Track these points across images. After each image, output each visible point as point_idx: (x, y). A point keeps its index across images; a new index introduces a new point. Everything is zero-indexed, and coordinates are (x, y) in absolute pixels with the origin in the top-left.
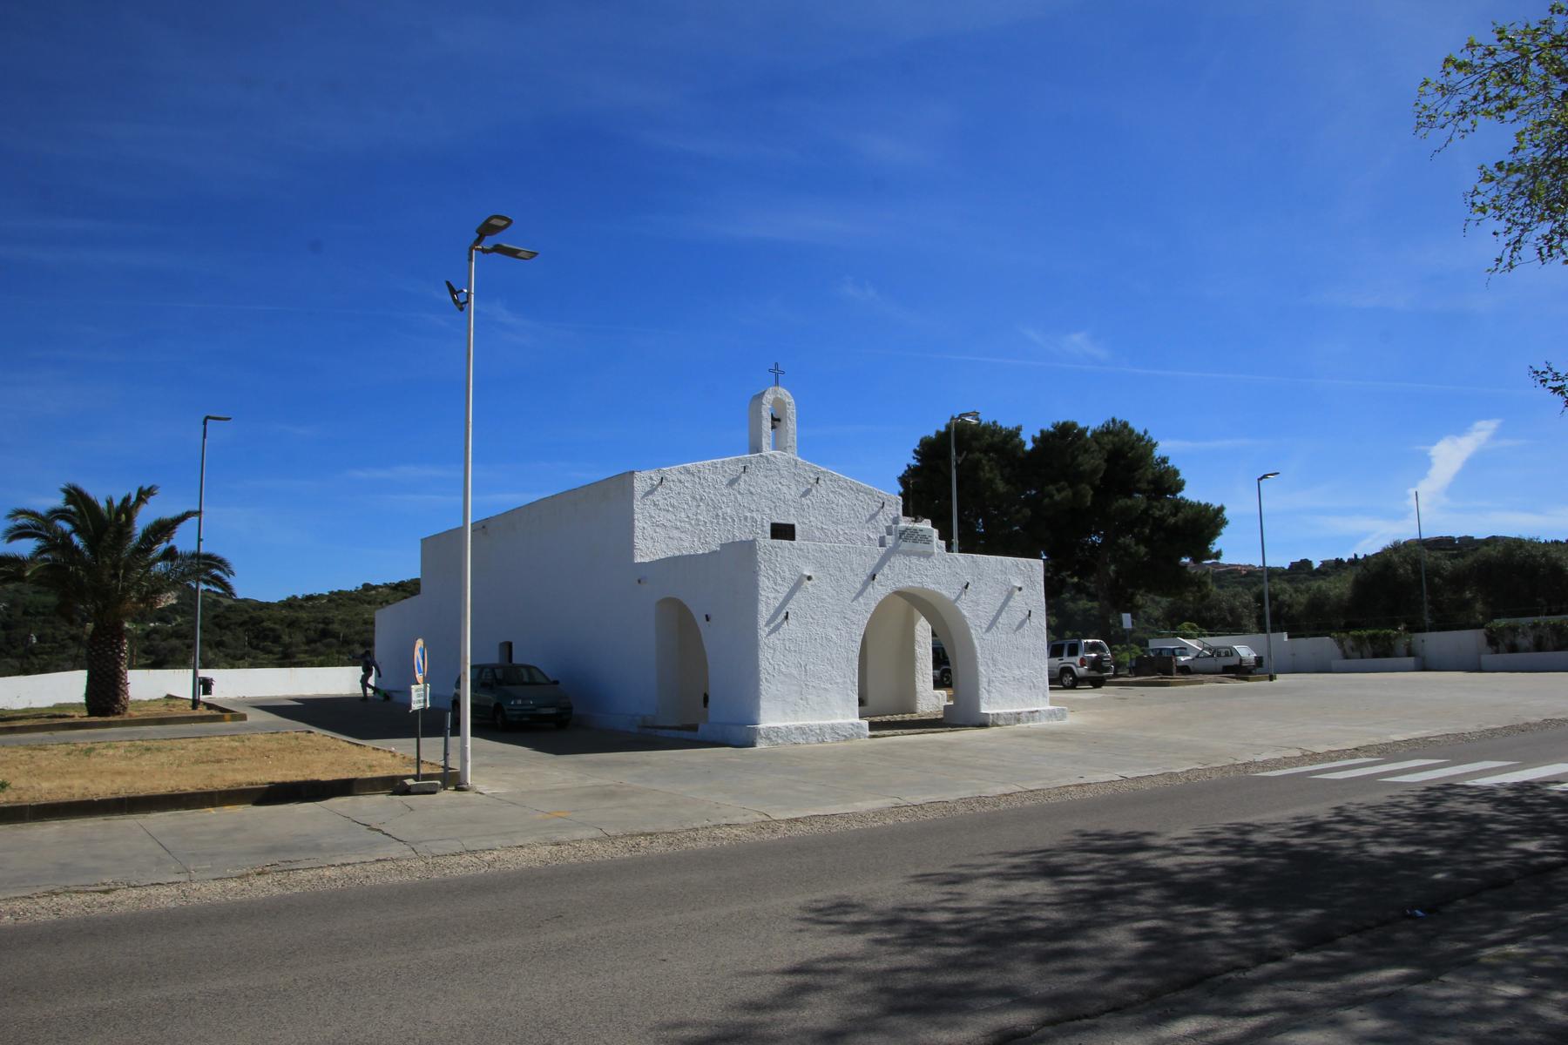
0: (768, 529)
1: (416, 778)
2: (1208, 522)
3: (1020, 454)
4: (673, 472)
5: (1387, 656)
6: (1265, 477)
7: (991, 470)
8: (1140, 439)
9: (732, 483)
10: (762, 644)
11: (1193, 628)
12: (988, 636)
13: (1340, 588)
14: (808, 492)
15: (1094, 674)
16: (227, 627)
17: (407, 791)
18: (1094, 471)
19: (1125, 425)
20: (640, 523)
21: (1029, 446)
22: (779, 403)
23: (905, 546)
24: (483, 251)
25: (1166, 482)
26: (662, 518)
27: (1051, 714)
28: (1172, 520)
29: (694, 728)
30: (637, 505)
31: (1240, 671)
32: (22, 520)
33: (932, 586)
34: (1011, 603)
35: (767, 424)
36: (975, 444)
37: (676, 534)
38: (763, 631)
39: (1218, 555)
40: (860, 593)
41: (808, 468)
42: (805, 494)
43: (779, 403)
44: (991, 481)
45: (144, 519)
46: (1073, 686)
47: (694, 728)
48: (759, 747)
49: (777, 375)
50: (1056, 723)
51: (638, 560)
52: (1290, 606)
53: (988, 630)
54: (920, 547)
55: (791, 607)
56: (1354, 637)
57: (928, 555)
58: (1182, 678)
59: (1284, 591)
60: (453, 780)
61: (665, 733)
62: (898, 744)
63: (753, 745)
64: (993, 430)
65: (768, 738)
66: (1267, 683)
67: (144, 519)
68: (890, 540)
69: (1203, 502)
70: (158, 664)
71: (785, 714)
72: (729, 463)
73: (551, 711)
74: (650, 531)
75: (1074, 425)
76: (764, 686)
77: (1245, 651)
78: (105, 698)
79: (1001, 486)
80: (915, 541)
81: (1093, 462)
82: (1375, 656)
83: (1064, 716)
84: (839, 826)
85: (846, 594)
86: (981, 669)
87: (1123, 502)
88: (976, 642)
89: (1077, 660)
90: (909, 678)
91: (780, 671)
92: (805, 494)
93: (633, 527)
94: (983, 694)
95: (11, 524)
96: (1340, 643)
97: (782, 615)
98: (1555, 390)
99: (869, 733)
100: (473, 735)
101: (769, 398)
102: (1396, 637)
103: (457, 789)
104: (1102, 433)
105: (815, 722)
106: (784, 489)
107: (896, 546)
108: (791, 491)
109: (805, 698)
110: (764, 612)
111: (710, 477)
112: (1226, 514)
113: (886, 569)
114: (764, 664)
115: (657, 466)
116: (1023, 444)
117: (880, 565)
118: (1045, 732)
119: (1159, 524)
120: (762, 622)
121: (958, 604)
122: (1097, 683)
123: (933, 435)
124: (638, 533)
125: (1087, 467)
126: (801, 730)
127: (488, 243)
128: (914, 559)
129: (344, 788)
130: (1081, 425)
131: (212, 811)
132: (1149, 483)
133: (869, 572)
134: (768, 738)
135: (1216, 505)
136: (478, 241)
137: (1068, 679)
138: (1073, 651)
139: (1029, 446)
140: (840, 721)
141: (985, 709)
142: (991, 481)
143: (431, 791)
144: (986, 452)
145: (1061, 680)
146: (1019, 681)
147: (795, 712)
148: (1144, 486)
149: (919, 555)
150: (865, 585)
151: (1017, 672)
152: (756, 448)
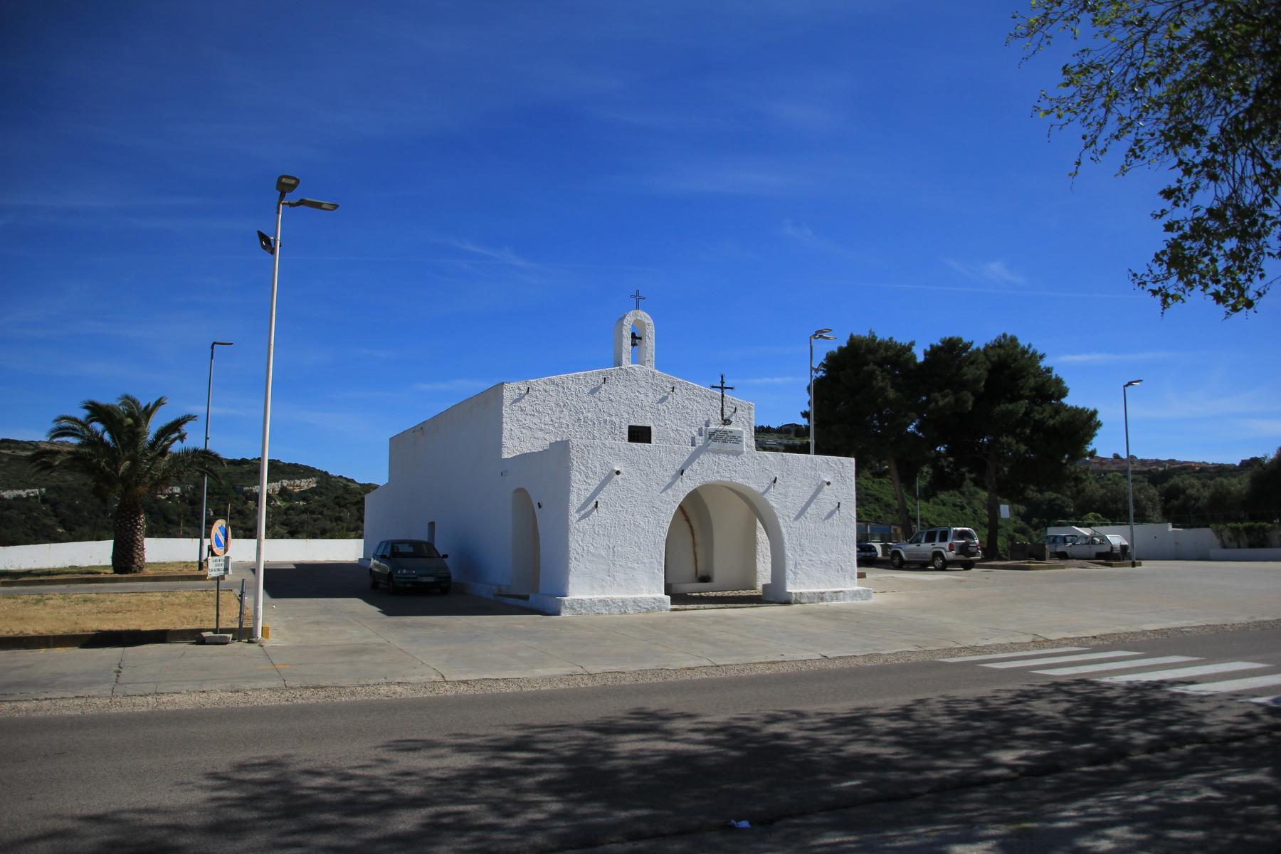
0: (626, 431)
1: (215, 631)
2: (1085, 424)
3: (911, 366)
4: (539, 383)
5: (1263, 546)
6: (1130, 384)
7: (884, 379)
8: (1024, 352)
9: (593, 392)
10: (572, 528)
11: (1096, 518)
13: (1239, 485)
14: (664, 399)
15: (962, 557)
16: (344, 506)
17: (202, 642)
18: (977, 381)
19: (1013, 339)
20: (507, 426)
21: (920, 358)
22: (638, 324)
23: (714, 445)
24: (291, 205)
25: (1050, 390)
26: (528, 421)
27: (856, 594)
28: (1051, 422)
29: (526, 598)
30: (506, 411)
31: (1110, 557)
32: (64, 424)
33: (740, 481)
34: (820, 496)
35: (627, 341)
36: (870, 357)
37: (540, 434)
38: (574, 516)
39: (1092, 454)
40: (669, 486)
41: (665, 379)
42: (661, 401)
43: (638, 324)
44: (883, 389)
45: (154, 426)
46: (943, 568)
47: (526, 598)
49: (638, 301)
50: (860, 602)
51: (505, 456)
52: (1197, 499)
53: (797, 518)
54: (729, 446)
55: (601, 497)
56: (1232, 529)
57: (738, 454)
58: (1058, 562)
59: (1192, 486)
60: (245, 634)
61: (510, 601)
63: (558, 614)
64: (889, 345)
65: (572, 608)
66: (1130, 569)
67: (154, 426)
68: (700, 441)
69: (1080, 407)
70: (293, 534)
72: (592, 376)
73: (430, 579)
74: (517, 432)
75: (960, 340)
76: (573, 564)
77: (1116, 538)
78: (126, 561)
79: (891, 394)
80: (724, 441)
81: (978, 373)
82: (1251, 546)
83: (869, 597)
84: (502, 688)
85: (655, 486)
86: (788, 553)
87: (1005, 407)
88: (784, 530)
89: (946, 545)
90: (707, 557)
92: (661, 401)
93: (501, 429)
95: (54, 426)
96: (1218, 533)
98: (1154, 293)
99: (670, 607)
101: (629, 320)
102: (1271, 529)
103: (250, 642)
104: (994, 347)
105: (617, 596)
106: (642, 397)
107: (706, 446)
108: (649, 399)
109: (613, 574)
110: (575, 501)
111: (573, 387)
112: (1099, 417)
114: (573, 545)
115: (519, 377)
116: (914, 357)
118: (846, 607)
119: (1038, 426)
120: (573, 510)
121: (766, 496)
122: (968, 566)
123: (836, 350)
124: (506, 433)
125: (969, 376)
126: (604, 603)
127: (291, 197)
128: (723, 457)
129: (159, 637)
130: (966, 340)
131: (43, 651)
132: (1031, 390)
133: (678, 467)
134: (572, 608)
135: (1092, 409)
136: (282, 196)
137: (939, 562)
138: (944, 538)
140: (645, 595)
141: (791, 588)
142: (883, 389)
143: (224, 642)
144: (880, 365)
145: (866, 560)
146: (827, 565)
147: (602, 587)
148: (1027, 393)
149: (728, 453)
150: (675, 478)
151: (824, 556)
152: (618, 363)
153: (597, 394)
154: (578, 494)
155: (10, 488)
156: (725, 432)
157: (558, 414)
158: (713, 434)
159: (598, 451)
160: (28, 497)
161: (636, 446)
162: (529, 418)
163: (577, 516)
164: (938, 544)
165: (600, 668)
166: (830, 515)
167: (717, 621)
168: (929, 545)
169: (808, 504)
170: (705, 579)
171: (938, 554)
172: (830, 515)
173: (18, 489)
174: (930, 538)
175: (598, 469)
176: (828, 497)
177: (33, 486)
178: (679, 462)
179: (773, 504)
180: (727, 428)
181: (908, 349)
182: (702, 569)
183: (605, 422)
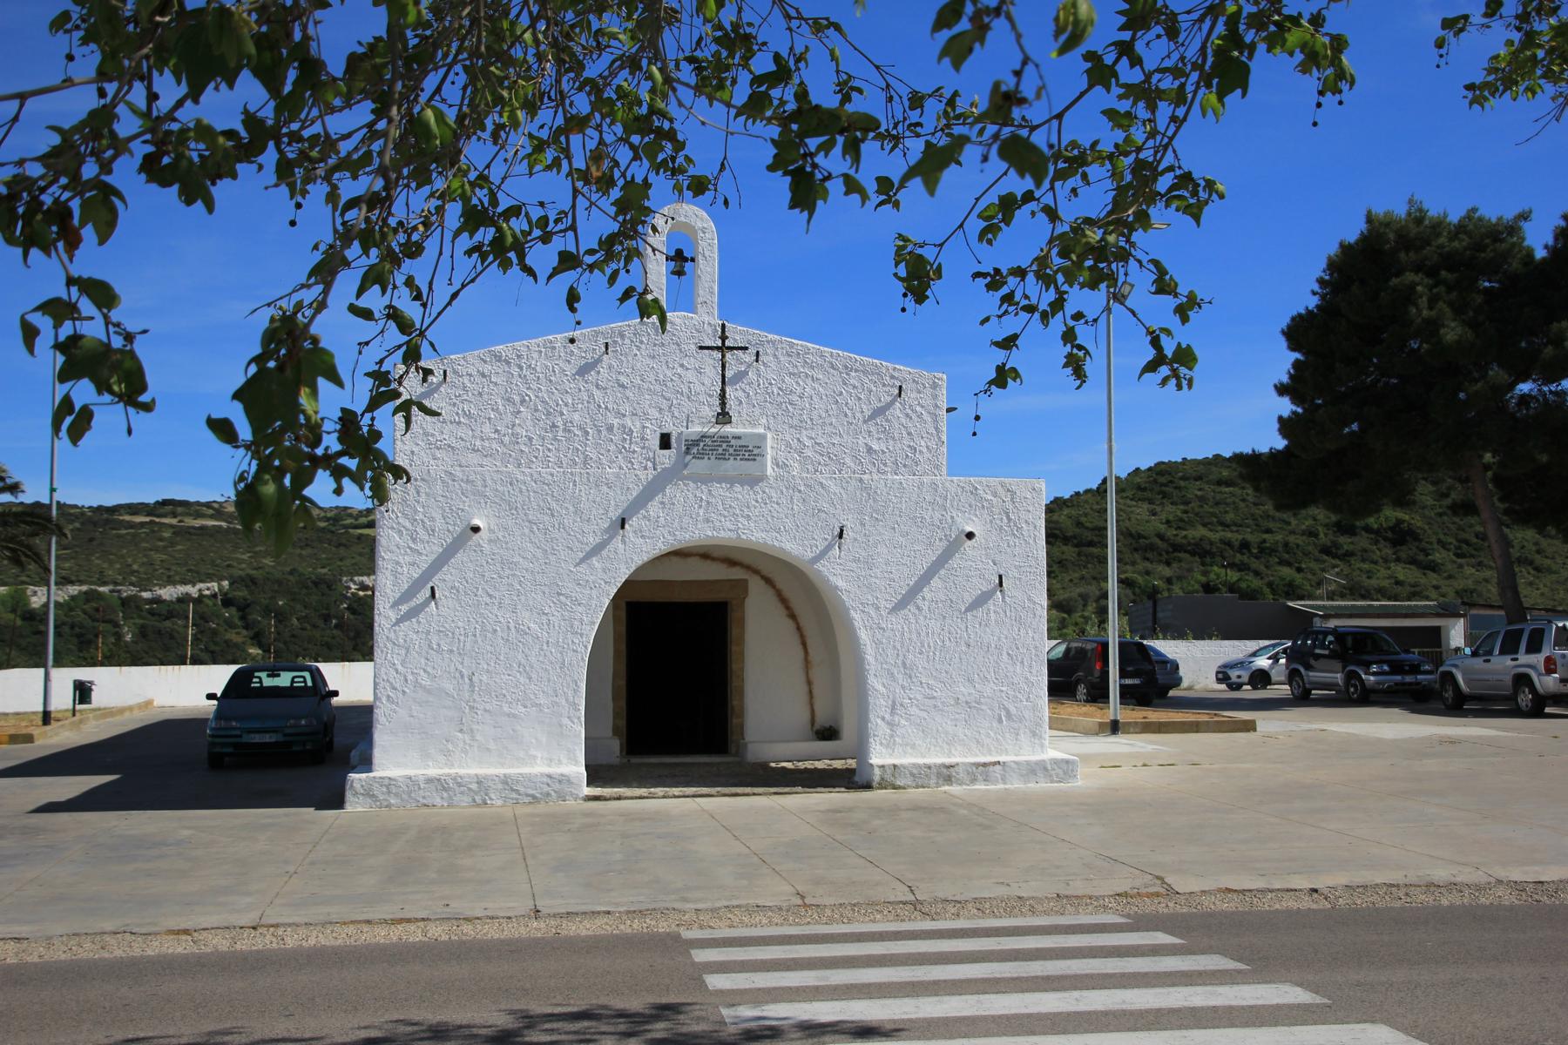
9: (583, 371)
12: (896, 622)
22: (683, 232)
23: (698, 466)
34: (955, 562)
40: (597, 550)
46: (1536, 710)
48: (349, 808)
55: (442, 580)
57: (754, 481)
62: (629, 817)
80: (722, 457)
86: (875, 683)
88: (863, 635)
89: (1538, 659)
91: (417, 684)
94: (878, 726)
97: (425, 590)
100: (370, 770)
105: (470, 769)
111: (540, 364)
113: (654, 508)
126: (438, 783)
128: (719, 489)
133: (615, 514)
137: (1525, 699)
139: (1540, 254)
144: (1432, 272)
146: (972, 706)
147: (447, 753)
149: (731, 481)
151: (963, 689)
154: (395, 574)
155: (171, 581)
156: (724, 439)
157: (509, 418)
158: (696, 443)
159: (439, 489)
160: (201, 596)
162: (448, 428)
163: (393, 616)
164: (1524, 658)
165: (425, 913)
166: (981, 601)
167: (286, 815)
168: (1507, 661)
169: (925, 579)
170: (828, 733)
171: (1522, 680)
172: (981, 601)
173: (184, 583)
174: (1510, 647)
175: (439, 523)
176: (974, 566)
177: (209, 577)
178: (617, 503)
179: (840, 583)
180: (728, 429)
181: (1513, 229)
182: (822, 720)
183: (610, 428)
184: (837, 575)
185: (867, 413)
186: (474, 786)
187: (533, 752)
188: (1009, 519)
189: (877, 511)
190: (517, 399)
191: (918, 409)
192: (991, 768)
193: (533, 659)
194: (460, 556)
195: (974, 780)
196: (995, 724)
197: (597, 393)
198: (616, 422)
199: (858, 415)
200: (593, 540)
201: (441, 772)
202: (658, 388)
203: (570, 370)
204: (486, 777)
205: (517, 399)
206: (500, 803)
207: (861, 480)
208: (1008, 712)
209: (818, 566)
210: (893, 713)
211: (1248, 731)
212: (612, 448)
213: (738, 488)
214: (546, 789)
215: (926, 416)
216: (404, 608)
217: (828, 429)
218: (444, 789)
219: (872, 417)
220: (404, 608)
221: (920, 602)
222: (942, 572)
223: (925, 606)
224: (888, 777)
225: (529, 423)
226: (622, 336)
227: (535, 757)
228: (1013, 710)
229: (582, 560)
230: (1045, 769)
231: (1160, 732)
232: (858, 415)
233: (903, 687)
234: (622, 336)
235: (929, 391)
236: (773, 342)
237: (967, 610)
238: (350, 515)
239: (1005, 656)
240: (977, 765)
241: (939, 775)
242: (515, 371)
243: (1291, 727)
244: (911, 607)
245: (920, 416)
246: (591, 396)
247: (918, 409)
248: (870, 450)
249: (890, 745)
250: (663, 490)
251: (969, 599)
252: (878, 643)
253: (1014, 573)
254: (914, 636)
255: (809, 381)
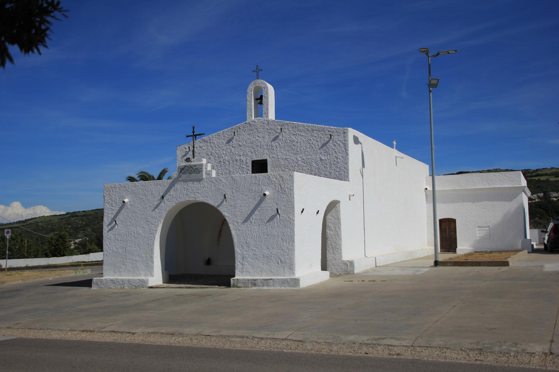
9: (228, 142)
14: (277, 137)
23: (184, 176)
34: (263, 205)
38: (106, 228)
49: (258, 73)
54: (194, 176)
57: (200, 180)
71: (115, 272)
72: (227, 132)
80: (190, 173)
88: (233, 232)
91: (113, 250)
106: (261, 139)
113: (172, 192)
117: (168, 191)
128: (190, 184)
147: (120, 272)
149: (193, 181)
153: (231, 143)
154: (108, 217)
156: (191, 167)
159: (118, 190)
161: (260, 176)
163: (107, 229)
166: (272, 218)
172: (272, 218)
183: (237, 160)
184: (225, 211)
185: (320, 146)
186: (121, 282)
187: (141, 272)
188: (281, 188)
189: (237, 188)
190: (210, 153)
191: (338, 142)
192: (269, 281)
193: (141, 242)
194: (123, 211)
195: (263, 286)
196: (277, 265)
197: (232, 149)
198: (238, 158)
199: (317, 147)
200: (156, 203)
201: (114, 278)
202: (251, 145)
203: (225, 142)
204: (124, 279)
205: (210, 153)
206: (127, 288)
207: (232, 177)
208: (280, 259)
209: (219, 209)
210: (243, 260)
211: (505, 266)
212: (237, 167)
213: (195, 183)
214: (139, 284)
215: (342, 145)
216: (110, 227)
217: (306, 153)
218: (114, 283)
219: (322, 147)
220: (110, 227)
221: (251, 220)
222: (259, 208)
223: (253, 221)
224: (236, 284)
225: (213, 161)
226: (240, 129)
227: (141, 274)
228: (282, 259)
229: (153, 210)
230: (288, 282)
231: (461, 266)
232: (317, 147)
233: (246, 251)
234: (240, 129)
235: (342, 135)
236: (287, 124)
237: (268, 222)
238: (530, 173)
239: (280, 239)
240: (264, 280)
241: (252, 283)
242: (209, 144)
243: (34, 274)
244: (249, 222)
245: (339, 145)
246: (231, 150)
247: (338, 142)
248: (321, 159)
249: (242, 272)
250: (174, 185)
251: (268, 218)
252: (238, 235)
253: (283, 208)
254: (250, 232)
255: (300, 137)
